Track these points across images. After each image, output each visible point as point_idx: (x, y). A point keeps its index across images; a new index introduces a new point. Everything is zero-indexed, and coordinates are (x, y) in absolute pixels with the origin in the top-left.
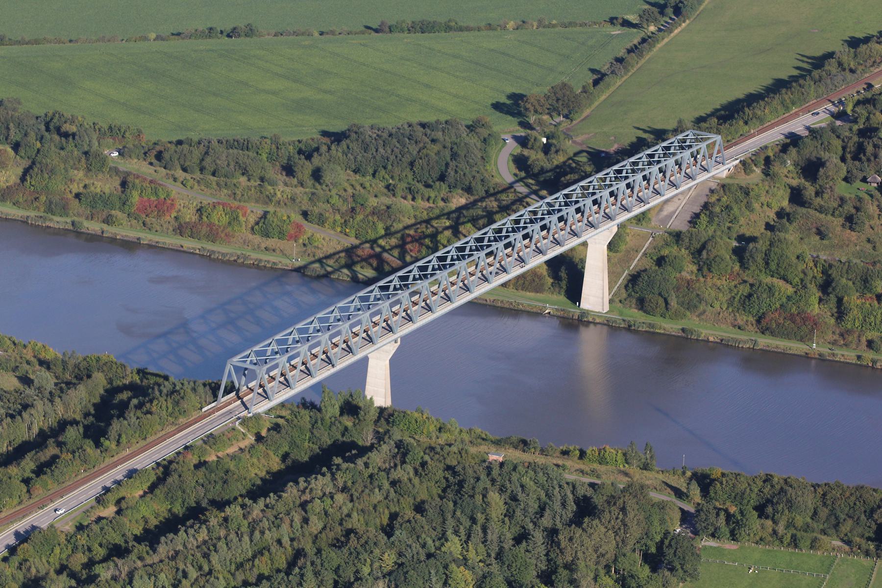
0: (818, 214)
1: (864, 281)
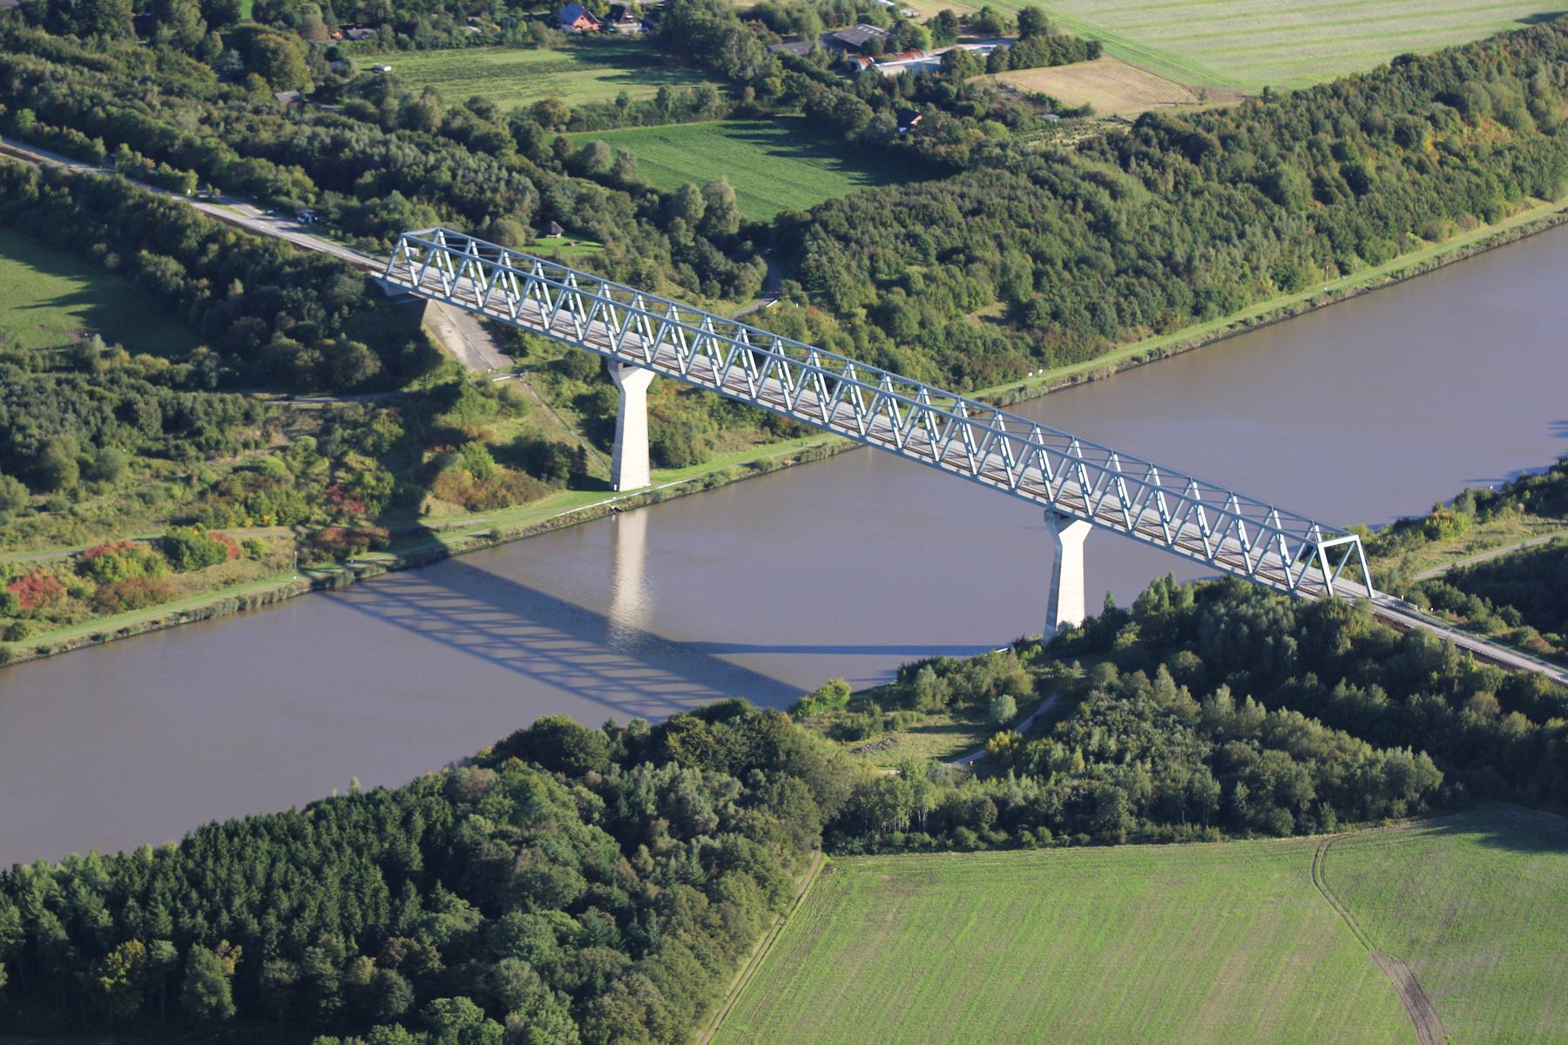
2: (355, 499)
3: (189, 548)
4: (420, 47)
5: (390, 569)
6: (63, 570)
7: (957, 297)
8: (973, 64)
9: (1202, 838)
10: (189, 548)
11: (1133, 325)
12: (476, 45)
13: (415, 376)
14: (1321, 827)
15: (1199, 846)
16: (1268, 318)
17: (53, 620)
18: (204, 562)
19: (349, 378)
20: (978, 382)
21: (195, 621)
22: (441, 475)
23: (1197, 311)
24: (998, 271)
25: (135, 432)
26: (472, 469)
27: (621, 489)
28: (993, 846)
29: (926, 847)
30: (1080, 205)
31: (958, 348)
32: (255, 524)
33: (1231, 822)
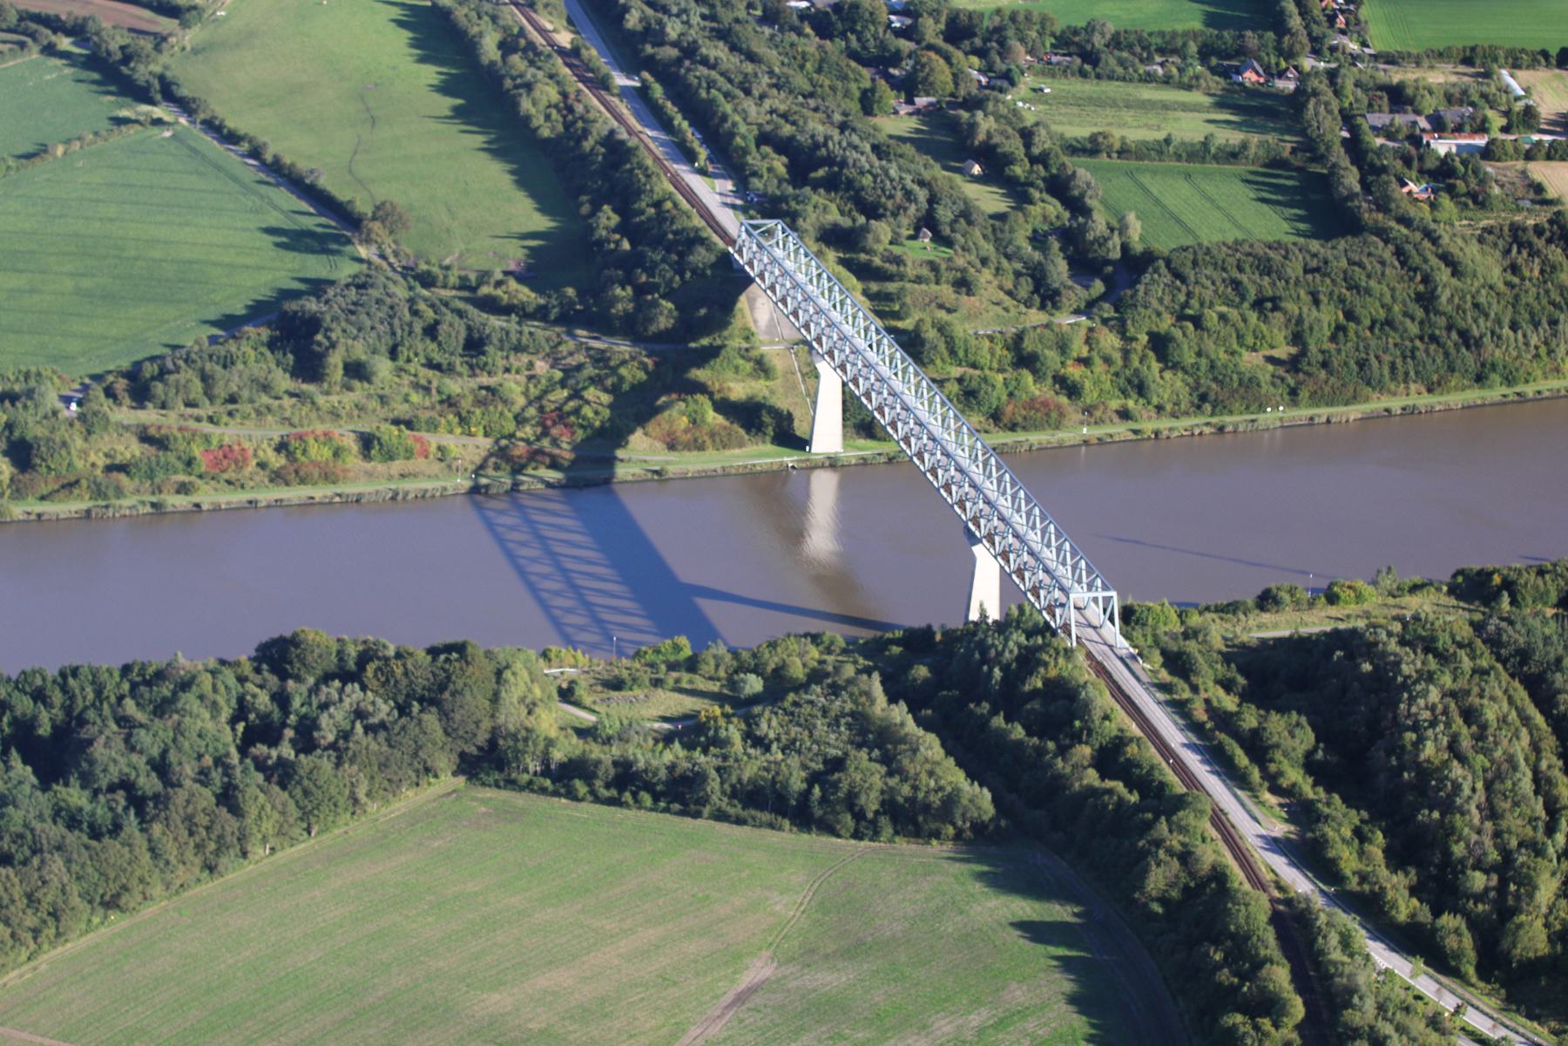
1: (1061, 348)
2: (566, 426)
4: (1098, 77)
5: (549, 485)
6: (265, 445)
7: (1240, 337)
8: (1511, 150)
9: (771, 826)
10: (380, 444)
11: (1406, 381)
13: (708, 335)
14: (875, 835)
15: (768, 832)
16: (1547, 394)
17: (229, 482)
18: (390, 457)
19: (646, 329)
20: (1217, 410)
22: (659, 417)
23: (1480, 379)
24: (1293, 321)
25: (434, 346)
26: (690, 415)
27: (813, 451)
28: (597, 799)
29: (543, 791)
30: (1419, 278)
31: (1215, 379)
32: (462, 433)
33: (802, 816)
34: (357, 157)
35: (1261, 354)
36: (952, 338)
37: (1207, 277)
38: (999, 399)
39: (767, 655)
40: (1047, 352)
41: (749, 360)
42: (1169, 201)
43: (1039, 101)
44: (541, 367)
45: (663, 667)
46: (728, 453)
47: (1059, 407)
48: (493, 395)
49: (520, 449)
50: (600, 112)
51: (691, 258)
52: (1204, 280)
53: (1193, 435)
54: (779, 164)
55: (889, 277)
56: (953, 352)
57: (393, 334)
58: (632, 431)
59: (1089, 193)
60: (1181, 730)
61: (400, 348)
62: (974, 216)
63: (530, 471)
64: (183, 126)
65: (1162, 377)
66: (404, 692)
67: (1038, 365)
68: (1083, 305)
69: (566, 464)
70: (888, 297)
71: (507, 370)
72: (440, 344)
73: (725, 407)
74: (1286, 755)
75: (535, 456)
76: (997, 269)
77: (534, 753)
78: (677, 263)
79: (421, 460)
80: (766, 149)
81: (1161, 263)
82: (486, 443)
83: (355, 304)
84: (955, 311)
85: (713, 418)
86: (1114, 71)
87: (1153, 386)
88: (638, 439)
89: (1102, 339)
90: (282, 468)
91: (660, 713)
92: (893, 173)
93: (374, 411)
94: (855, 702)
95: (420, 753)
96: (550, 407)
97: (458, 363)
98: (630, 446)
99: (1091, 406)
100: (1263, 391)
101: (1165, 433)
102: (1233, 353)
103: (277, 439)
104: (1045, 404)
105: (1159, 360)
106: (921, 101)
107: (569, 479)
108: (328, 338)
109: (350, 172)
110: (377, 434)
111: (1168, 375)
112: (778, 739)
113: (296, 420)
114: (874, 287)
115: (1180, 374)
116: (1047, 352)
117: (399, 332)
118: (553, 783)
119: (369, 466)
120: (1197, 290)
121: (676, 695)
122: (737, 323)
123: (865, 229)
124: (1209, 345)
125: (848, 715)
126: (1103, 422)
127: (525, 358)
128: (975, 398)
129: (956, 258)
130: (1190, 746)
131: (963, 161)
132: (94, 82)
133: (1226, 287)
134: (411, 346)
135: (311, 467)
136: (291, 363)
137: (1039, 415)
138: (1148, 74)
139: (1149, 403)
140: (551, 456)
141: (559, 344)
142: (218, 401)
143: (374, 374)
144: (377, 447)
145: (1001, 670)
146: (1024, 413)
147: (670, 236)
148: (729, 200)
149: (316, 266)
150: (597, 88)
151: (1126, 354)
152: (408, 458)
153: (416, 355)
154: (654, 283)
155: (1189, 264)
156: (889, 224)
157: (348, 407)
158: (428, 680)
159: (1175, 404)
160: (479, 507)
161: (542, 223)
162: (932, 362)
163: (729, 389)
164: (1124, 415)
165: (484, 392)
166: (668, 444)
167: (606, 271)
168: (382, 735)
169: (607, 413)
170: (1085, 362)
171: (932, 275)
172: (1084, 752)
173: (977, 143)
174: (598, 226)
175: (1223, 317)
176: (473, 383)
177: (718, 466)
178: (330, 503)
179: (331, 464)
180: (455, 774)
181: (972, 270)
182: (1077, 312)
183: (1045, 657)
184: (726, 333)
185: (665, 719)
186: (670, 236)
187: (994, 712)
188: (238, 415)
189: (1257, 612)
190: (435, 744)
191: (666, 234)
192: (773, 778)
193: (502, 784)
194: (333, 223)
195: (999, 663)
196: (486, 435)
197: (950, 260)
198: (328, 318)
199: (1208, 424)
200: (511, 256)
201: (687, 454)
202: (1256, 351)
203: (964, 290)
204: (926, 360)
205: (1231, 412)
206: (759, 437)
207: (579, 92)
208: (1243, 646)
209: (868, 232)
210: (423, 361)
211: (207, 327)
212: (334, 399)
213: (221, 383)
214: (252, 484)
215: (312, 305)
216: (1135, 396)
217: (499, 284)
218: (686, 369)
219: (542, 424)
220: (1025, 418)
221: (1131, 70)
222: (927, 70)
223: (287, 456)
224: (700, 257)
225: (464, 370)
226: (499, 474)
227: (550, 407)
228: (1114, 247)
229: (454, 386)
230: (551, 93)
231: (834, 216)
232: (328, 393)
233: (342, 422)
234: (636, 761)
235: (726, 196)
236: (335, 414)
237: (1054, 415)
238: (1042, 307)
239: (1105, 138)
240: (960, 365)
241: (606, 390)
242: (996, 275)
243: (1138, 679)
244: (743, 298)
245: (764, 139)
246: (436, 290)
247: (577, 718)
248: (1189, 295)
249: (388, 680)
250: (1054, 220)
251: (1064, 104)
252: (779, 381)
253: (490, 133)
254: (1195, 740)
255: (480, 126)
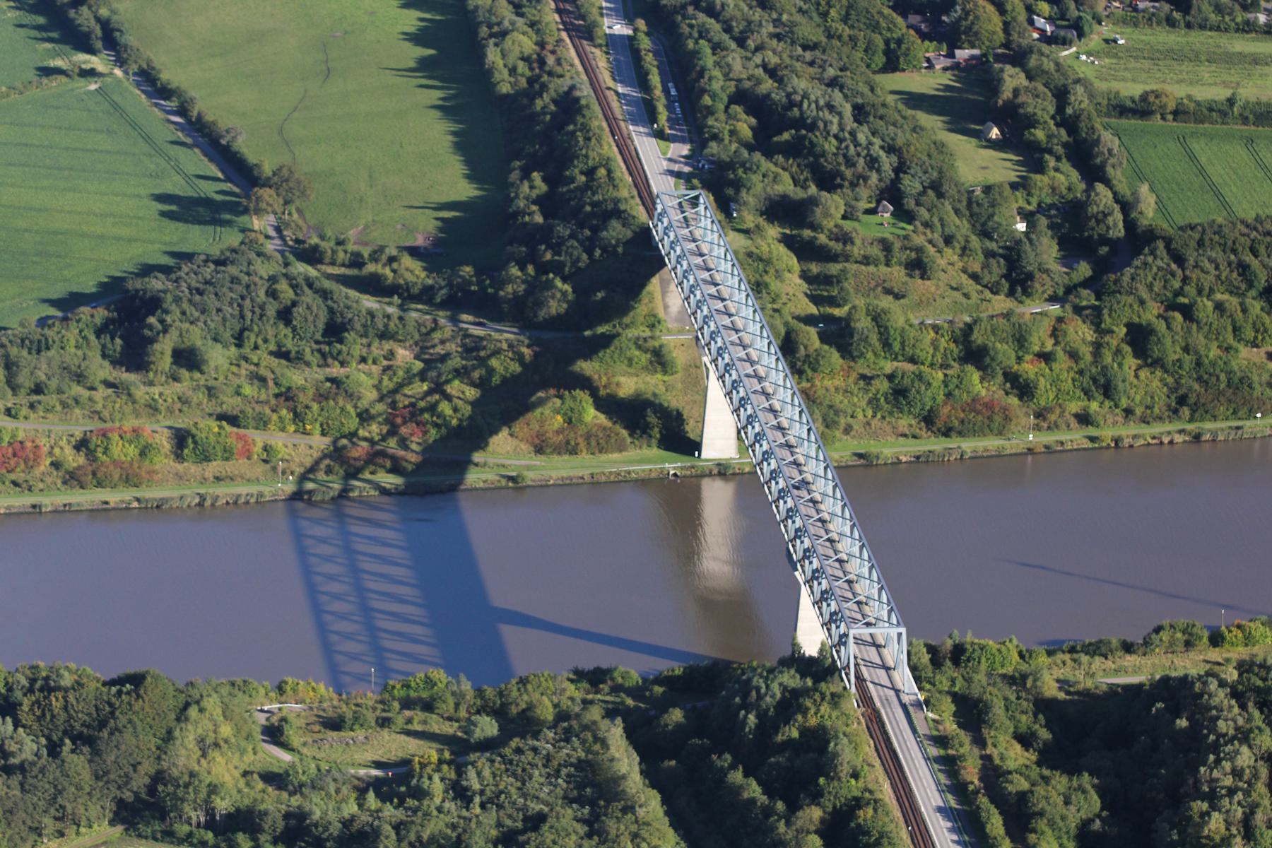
0: (863, 267)
1: (1018, 341)
2: (418, 424)
3: (195, 442)
4: (1189, 26)
5: (384, 492)
6: (63, 443)
7: (1236, 330)
10: (195, 442)
12: (1244, 31)
13: (606, 320)
17: (15, 484)
18: (205, 458)
19: (536, 316)
20: (1197, 415)
21: (146, 508)
22: (529, 416)
25: (288, 331)
26: (565, 414)
27: (704, 456)
34: (296, 115)
35: (1263, 350)
36: (886, 328)
37: (1210, 260)
38: (934, 399)
39: (515, 693)
40: (998, 345)
41: (646, 351)
42: (1217, 172)
43: (1108, 55)
44: (404, 355)
45: (396, 705)
46: (604, 457)
47: (1005, 409)
48: (338, 387)
49: (360, 450)
50: (572, 65)
51: (605, 233)
52: (1207, 265)
53: (1162, 443)
54: (745, 126)
55: (832, 257)
56: (886, 345)
57: (242, 317)
58: (495, 431)
59: (1111, 161)
60: (941, 792)
61: (246, 333)
62: (945, 187)
63: (367, 476)
64: (116, 78)
65: (1137, 376)
66: (62, 728)
67: (988, 360)
68: (1061, 292)
69: (410, 467)
70: (827, 280)
71: (363, 360)
72: (294, 330)
73: (611, 405)
74: (1051, 823)
75: (375, 457)
76: (964, 249)
77: (195, 801)
78: (588, 239)
79: (243, 461)
80: (737, 109)
81: (1161, 245)
82: (320, 443)
83: (207, 282)
84: (903, 297)
85: (592, 415)
86: (1206, 20)
87: (1121, 386)
88: (501, 442)
89: (1071, 330)
90: (79, 468)
91: (376, 758)
92: (861, 137)
93: (199, 404)
94: (588, 751)
95: (59, 799)
96: (402, 401)
97: (308, 350)
98: (490, 448)
99: (1045, 409)
100: (1257, 393)
101: (1126, 442)
102: (1228, 349)
103: (78, 435)
104: (989, 406)
105: (1136, 356)
106: (962, 54)
107: (407, 485)
108: (162, 321)
109: (281, 132)
110: (194, 431)
111: (1144, 374)
112: (482, 793)
113: (106, 414)
114: (815, 268)
115: (1159, 373)
116: (998, 345)
117: (249, 315)
118: (216, 835)
119: (180, 467)
120: (1194, 275)
121: (403, 737)
122: (641, 309)
123: (813, 202)
124: (1199, 339)
125: (572, 765)
126: (1057, 426)
127: (387, 345)
128: (905, 397)
129: (914, 236)
130: (944, 811)
131: (982, 123)
132: (38, 28)
133: (1232, 271)
134: (260, 331)
135: (111, 468)
136: (118, 349)
137: (980, 418)
138: (1247, 23)
139: (1116, 406)
140: (394, 459)
141: (433, 330)
142: (23, 391)
143: (205, 362)
144: (191, 446)
145: (757, 717)
146: (962, 415)
147: (588, 208)
148: (676, 168)
149: (199, 239)
150: (579, 38)
151: (1097, 347)
152: (227, 459)
153: (266, 341)
154: (559, 262)
155: (1193, 244)
156: (843, 196)
157: (170, 400)
158: (89, 715)
159: (1147, 407)
160: (293, 515)
161: (465, 191)
162: (862, 355)
163: (618, 384)
164: (1084, 419)
165: (328, 384)
166: (536, 447)
167: (509, 248)
168: (15, 780)
169: (467, 410)
170: (1046, 357)
171: (881, 255)
172: (814, 814)
173: (1000, 102)
174: (517, 196)
175: (1219, 307)
176: (318, 374)
177: (586, 473)
178: (127, 509)
179: (136, 465)
180: (112, 823)
181: (931, 250)
182: (1053, 299)
183: (808, 703)
184: (627, 320)
185: (378, 765)
186: (588, 208)
187: (733, 767)
188: (40, 407)
189: (1120, 653)
190: (79, 788)
191: (583, 206)
192: (459, 837)
193: (159, 836)
194: (236, 190)
195: (758, 707)
196: (323, 434)
197: (906, 237)
198: (169, 298)
199: (1181, 431)
200: (421, 228)
201: (556, 458)
202: (1257, 346)
203: (917, 272)
204: (855, 354)
205: (1215, 418)
206: (644, 441)
207: (560, 41)
208: (1086, 694)
209: (817, 206)
210: (272, 347)
211: (45, 306)
212: (156, 390)
213: (25, 372)
214: (41, 485)
215: (157, 283)
216: (1101, 398)
217: (392, 259)
218: (573, 360)
219: (390, 421)
220: (962, 422)
221: (1227, 18)
222: (971, 18)
223: (86, 455)
224: (615, 232)
225: (315, 359)
226: (330, 478)
227: (402, 401)
228: (1115, 225)
229: (296, 377)
230: (524, 42)
231: (786, 186)
232: (151, 384)
233: (160, 417)
234: (310, 813)
235: (675, 162)
236: (153, 408)
237: (998, 419)
238: (1011, 293)
239: (1157, 97)
240: (896, 359)
241: (473, 384)
242: (962, 255)
243: (914, 730)
244: (655, 280)
245: (742, 97)
246: (323, 268)
247: (273, 757)
248: (1185, 280)
249: (44, 715)
250: (1065, 192)
251: (1136, 58)
252: (678, 376)
253: (448, 88)
254: (953, 803)
255: (441, 81)
